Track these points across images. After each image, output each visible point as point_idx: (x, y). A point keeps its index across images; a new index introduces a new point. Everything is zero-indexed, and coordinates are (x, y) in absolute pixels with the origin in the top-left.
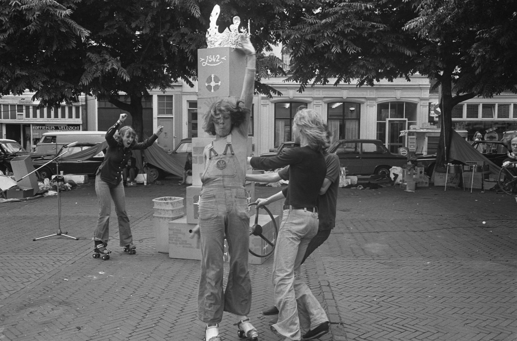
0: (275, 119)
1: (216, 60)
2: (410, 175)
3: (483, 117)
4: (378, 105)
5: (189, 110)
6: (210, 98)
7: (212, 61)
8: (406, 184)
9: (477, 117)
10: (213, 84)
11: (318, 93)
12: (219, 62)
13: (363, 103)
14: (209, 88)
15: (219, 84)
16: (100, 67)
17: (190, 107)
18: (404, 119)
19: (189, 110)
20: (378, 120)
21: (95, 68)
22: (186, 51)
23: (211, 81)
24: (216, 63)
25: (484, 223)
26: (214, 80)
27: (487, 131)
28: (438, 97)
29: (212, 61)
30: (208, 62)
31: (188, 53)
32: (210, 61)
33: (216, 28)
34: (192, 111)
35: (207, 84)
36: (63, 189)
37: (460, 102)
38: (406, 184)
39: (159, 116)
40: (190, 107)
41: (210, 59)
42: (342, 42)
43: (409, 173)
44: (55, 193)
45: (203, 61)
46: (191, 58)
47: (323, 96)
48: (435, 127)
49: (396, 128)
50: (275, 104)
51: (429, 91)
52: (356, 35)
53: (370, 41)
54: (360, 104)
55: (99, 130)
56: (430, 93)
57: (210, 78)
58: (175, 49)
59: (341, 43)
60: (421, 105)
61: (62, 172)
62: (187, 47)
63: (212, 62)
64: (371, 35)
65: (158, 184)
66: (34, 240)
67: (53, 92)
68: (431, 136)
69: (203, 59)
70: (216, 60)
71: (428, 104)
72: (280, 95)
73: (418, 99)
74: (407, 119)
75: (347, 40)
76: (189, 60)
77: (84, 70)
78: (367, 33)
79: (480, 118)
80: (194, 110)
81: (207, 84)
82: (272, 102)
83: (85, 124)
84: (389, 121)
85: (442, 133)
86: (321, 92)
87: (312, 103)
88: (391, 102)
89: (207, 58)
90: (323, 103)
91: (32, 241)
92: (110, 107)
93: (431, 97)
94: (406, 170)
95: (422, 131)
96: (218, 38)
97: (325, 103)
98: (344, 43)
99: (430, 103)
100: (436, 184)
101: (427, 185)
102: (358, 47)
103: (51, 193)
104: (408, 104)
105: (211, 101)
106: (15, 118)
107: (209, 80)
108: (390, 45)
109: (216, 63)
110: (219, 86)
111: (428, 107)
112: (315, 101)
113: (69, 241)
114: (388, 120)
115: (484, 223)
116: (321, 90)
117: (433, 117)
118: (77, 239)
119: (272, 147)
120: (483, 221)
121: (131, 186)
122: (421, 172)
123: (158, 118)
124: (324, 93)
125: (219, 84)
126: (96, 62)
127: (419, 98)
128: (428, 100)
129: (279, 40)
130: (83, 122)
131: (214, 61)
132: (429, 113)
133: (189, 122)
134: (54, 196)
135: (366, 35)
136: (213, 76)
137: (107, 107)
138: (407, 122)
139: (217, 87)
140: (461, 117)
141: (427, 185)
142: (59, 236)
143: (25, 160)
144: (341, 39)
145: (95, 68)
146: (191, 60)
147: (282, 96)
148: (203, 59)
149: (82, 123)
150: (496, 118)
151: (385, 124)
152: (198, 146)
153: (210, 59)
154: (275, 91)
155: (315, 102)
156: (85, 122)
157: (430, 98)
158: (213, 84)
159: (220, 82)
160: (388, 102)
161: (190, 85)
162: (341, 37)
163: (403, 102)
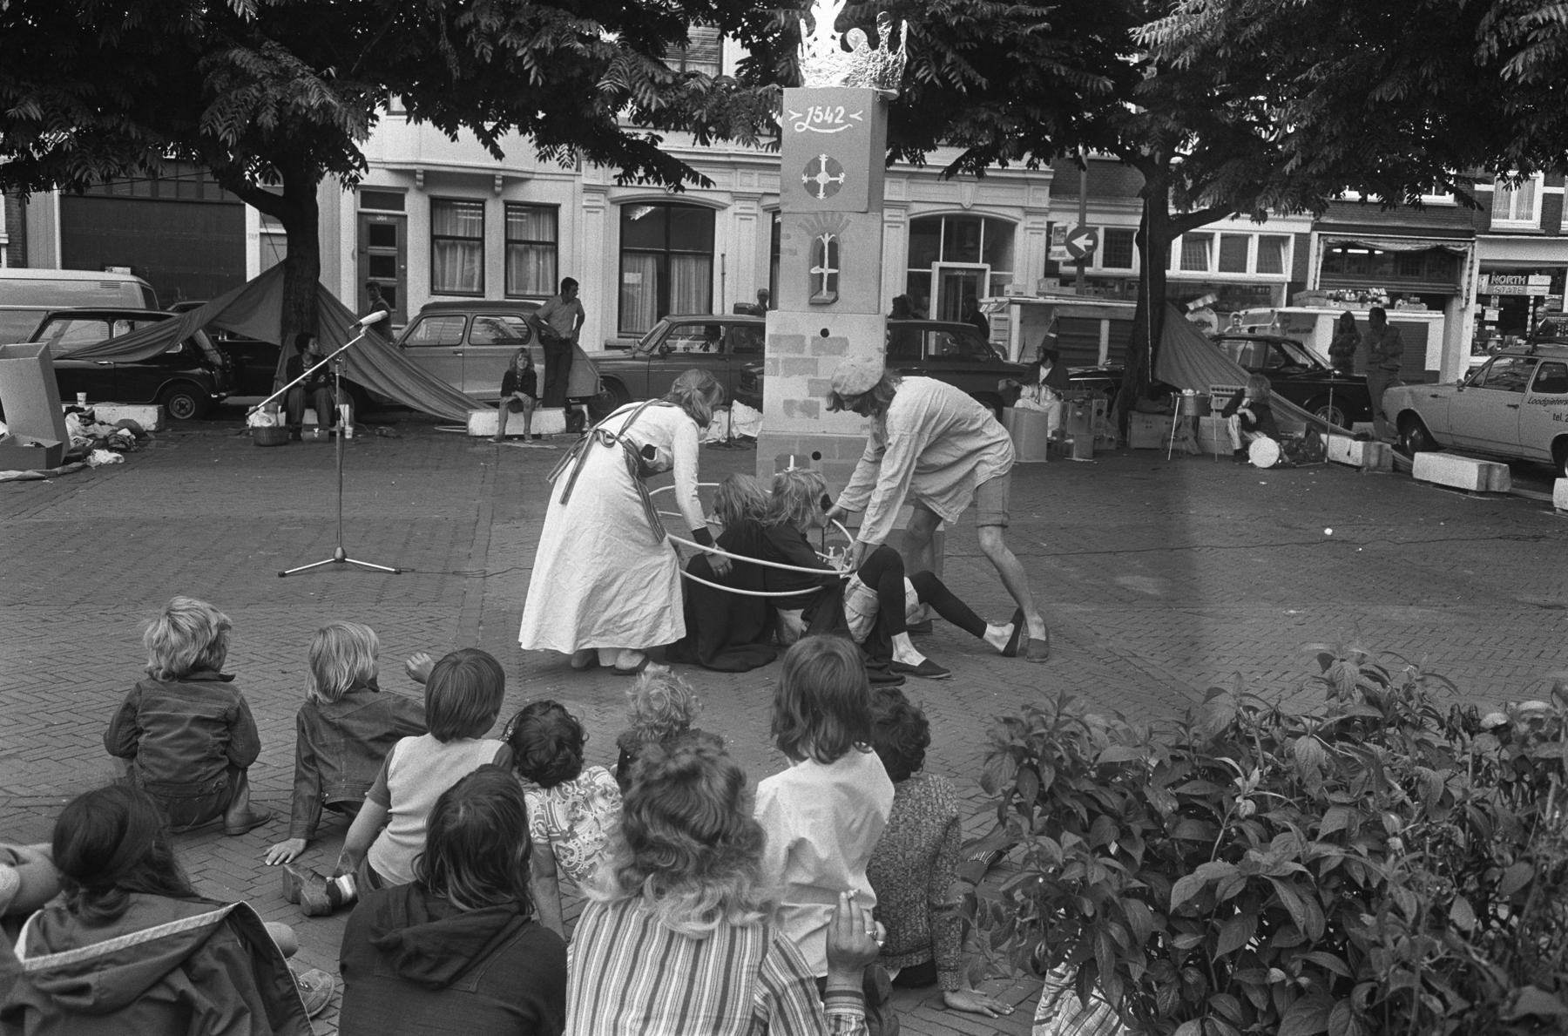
0: (622, 252)
1: (834, 118)
2: (1080, 418)
3: (1105, 265)
4: (913, 222)
5: (360, 214)
6: (816, 213)
7: (824, 121)
8: (1071, 441)
9: (1244, 270)
10: (823, 178)
11: (746, 180)
12: (842, 125)
13: (724, 207)
14: (812, 188)
15: (841, 178)
16: (273, 92)
17: (362, 206)
18: (980, 265)
19: (360, 214)
20: (910, 266)
21: (257, 94)
22: (520, 53)
23: (819, 170)
24: (833, 126)
25: (1328, 531)
26: (827, 170)
27: (1191, 306)
28: (1077, 207)
29: (824, 121)
30: (812, 123)
31: (526, 59)
32: (818, 121)
33: (833, 37)
34: (371, 219)
35: (805, 179)
36: (121, 446)
37: (1196, 227)
38: (1071, 441)
39: (264, 231)
40: (362, 206)
41: (818, 116)
42: (943, 56)
43: (1079, 414)
44: (117, 458)
45: (799, 119)
46: (537, 74)
47: (762, 191)
48: (1069, 290)
49: (963, 291)
50: (622, 206)
51: (1047, 190)
52: (977, 40)
53: (1013, 57)
54: (714, 211)
55: (64, 267)
56: (1051, 194)
57: (817, 162)
58: (483, 47)
59: (939, 58)
60: (1026, 229)
61: (81, 396)
62: (522, 42)
63: (824, 125)
64: (1011, 43)
65: (386, 436)
66: (283, 575)
67: (114, 155)
68: (1066, 315)
69: (796, 115)
70: (834, 118)
71: (1045, 226)
72: (708, 186)
73: (1020, 210)
74: (987, 266)
75: (955, 52)
76: (532, 77)
77: (212, 94)
78: (1002, 34)
79: (1251, 274)
80: (376, 215)
81: (805, 179)
82: (613, 202)
83: (19, 247)
84: (941, 269)
85: (1140, 310)
86: (756, 177)
87: (730, 210)
88: (947, 217)
89: (808, 113)
90: (761, 212)
91: (276, 578)
92: (217, 199)
93: (1054, 206)
94: (1070, 406)
95: (1041, 300)
96: (840, 64)
97: (765, 210)
98: (948, 60)
99: (1050, 224)
100: (1135, 444)
101: (1113, 447)
102: (983, 76)
103: (102, 456)
104: (992, 223)
105: (819, 222)
106: (1477, 302)
107: (813, 168)
108: (1058, 70)
109: (833, 126)
110: (840, 186)
111: (1044, 233)
112: (739, 204)
113: (369, 576)
114: (936, 265)
115: (1328, 531)
116: (757, 172)
117: (1056, 264)
118: (396, 573)
119: (613, 336)
120: (1326, 527)
121: (313, 441)
122: (1099, 412)
123: (262, 234)
124: (765, 180)
125: (841, 178)
126: (260, 76)
127: (1022, 207)
128: (1046, 214)
129: (731, 33)
130: (9, 238)
131: (830, 121)
132: (1048, 250)
133: (360, 252)
134: (112, 467)
135: (1001, 40)
136: (823, 159)
137: (181, 198)
138: (988, 273)
139: (832, 188)
140: (1244, 270)
141: (1113, 447)
142: (339, 565)
143: (40, 357)
144: (940, 47)
145: (257, 94)
146: (536, 80)
147: (712, 187)
148: (796, 115)
149: (6, 242)
150: (1213, 272)
151: (928, 277)
152: (781, 332)
153: (818, 116)
154: (695, 177)
155: (737, 207)
156: (17, 239)
157: (1051, 210)
158: (823, 178)
159: (843, 176)
160: (940, 217)
161: (492, 152)
162: (940, 43)
163: (977, 219)
